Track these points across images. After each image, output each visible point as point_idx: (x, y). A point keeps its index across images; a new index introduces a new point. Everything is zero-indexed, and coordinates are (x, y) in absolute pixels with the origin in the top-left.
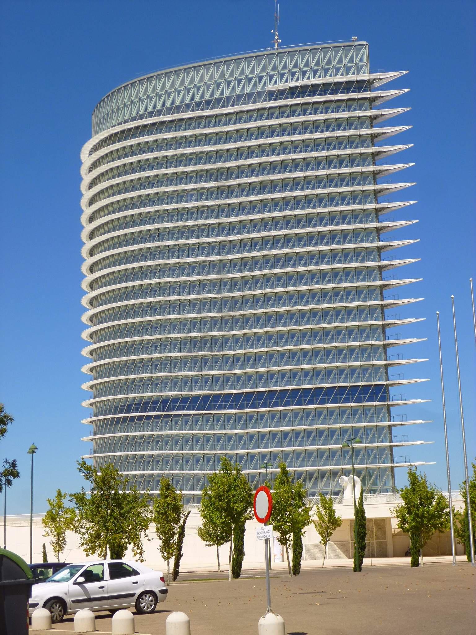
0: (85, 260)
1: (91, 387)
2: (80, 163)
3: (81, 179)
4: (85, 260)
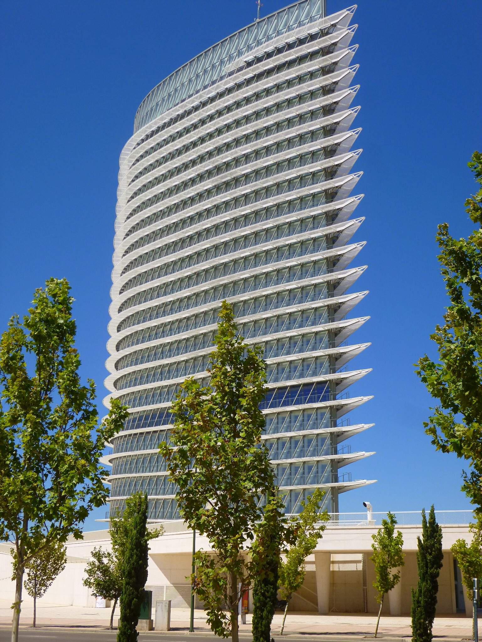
0: (109, 374)
1: (110, 461)
2: (112, 250)
3: (108, 318)
4: (109, 374)
